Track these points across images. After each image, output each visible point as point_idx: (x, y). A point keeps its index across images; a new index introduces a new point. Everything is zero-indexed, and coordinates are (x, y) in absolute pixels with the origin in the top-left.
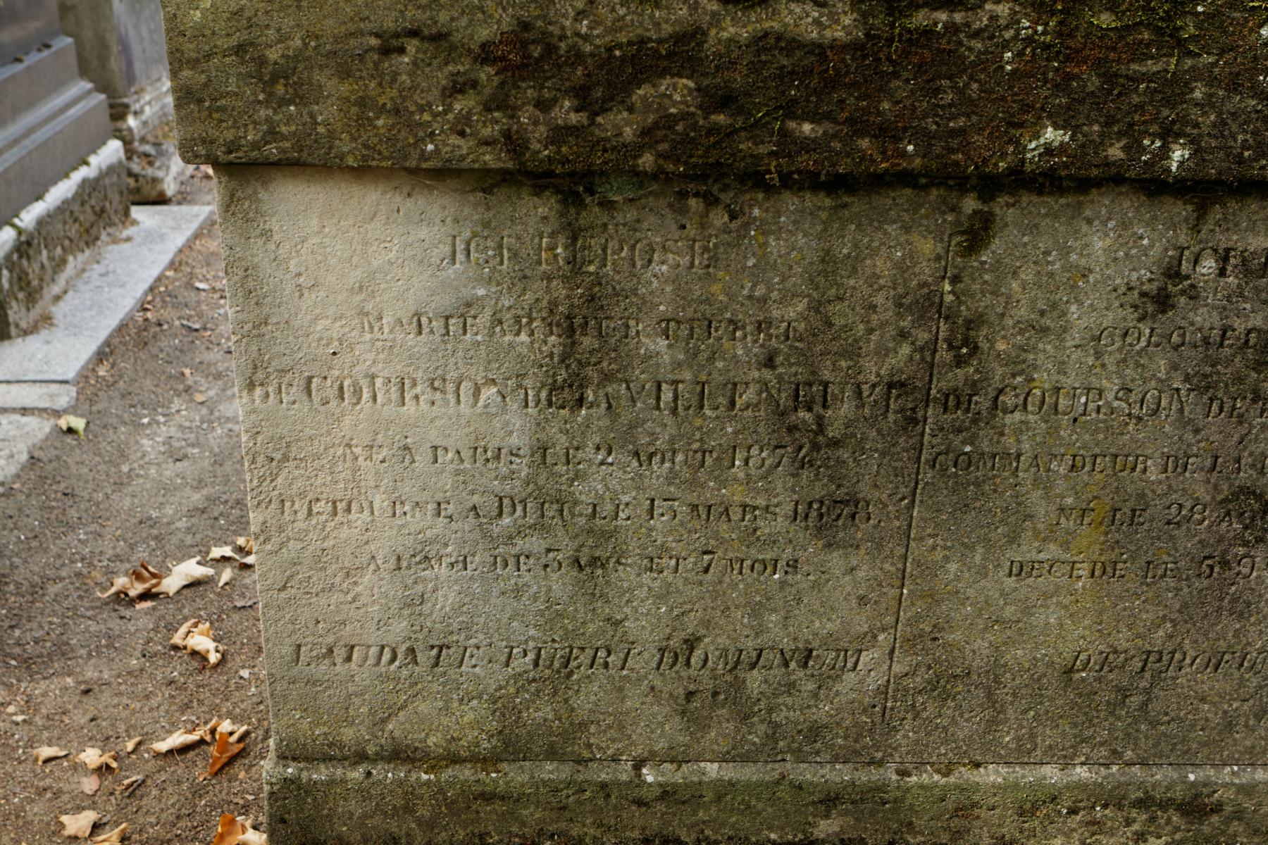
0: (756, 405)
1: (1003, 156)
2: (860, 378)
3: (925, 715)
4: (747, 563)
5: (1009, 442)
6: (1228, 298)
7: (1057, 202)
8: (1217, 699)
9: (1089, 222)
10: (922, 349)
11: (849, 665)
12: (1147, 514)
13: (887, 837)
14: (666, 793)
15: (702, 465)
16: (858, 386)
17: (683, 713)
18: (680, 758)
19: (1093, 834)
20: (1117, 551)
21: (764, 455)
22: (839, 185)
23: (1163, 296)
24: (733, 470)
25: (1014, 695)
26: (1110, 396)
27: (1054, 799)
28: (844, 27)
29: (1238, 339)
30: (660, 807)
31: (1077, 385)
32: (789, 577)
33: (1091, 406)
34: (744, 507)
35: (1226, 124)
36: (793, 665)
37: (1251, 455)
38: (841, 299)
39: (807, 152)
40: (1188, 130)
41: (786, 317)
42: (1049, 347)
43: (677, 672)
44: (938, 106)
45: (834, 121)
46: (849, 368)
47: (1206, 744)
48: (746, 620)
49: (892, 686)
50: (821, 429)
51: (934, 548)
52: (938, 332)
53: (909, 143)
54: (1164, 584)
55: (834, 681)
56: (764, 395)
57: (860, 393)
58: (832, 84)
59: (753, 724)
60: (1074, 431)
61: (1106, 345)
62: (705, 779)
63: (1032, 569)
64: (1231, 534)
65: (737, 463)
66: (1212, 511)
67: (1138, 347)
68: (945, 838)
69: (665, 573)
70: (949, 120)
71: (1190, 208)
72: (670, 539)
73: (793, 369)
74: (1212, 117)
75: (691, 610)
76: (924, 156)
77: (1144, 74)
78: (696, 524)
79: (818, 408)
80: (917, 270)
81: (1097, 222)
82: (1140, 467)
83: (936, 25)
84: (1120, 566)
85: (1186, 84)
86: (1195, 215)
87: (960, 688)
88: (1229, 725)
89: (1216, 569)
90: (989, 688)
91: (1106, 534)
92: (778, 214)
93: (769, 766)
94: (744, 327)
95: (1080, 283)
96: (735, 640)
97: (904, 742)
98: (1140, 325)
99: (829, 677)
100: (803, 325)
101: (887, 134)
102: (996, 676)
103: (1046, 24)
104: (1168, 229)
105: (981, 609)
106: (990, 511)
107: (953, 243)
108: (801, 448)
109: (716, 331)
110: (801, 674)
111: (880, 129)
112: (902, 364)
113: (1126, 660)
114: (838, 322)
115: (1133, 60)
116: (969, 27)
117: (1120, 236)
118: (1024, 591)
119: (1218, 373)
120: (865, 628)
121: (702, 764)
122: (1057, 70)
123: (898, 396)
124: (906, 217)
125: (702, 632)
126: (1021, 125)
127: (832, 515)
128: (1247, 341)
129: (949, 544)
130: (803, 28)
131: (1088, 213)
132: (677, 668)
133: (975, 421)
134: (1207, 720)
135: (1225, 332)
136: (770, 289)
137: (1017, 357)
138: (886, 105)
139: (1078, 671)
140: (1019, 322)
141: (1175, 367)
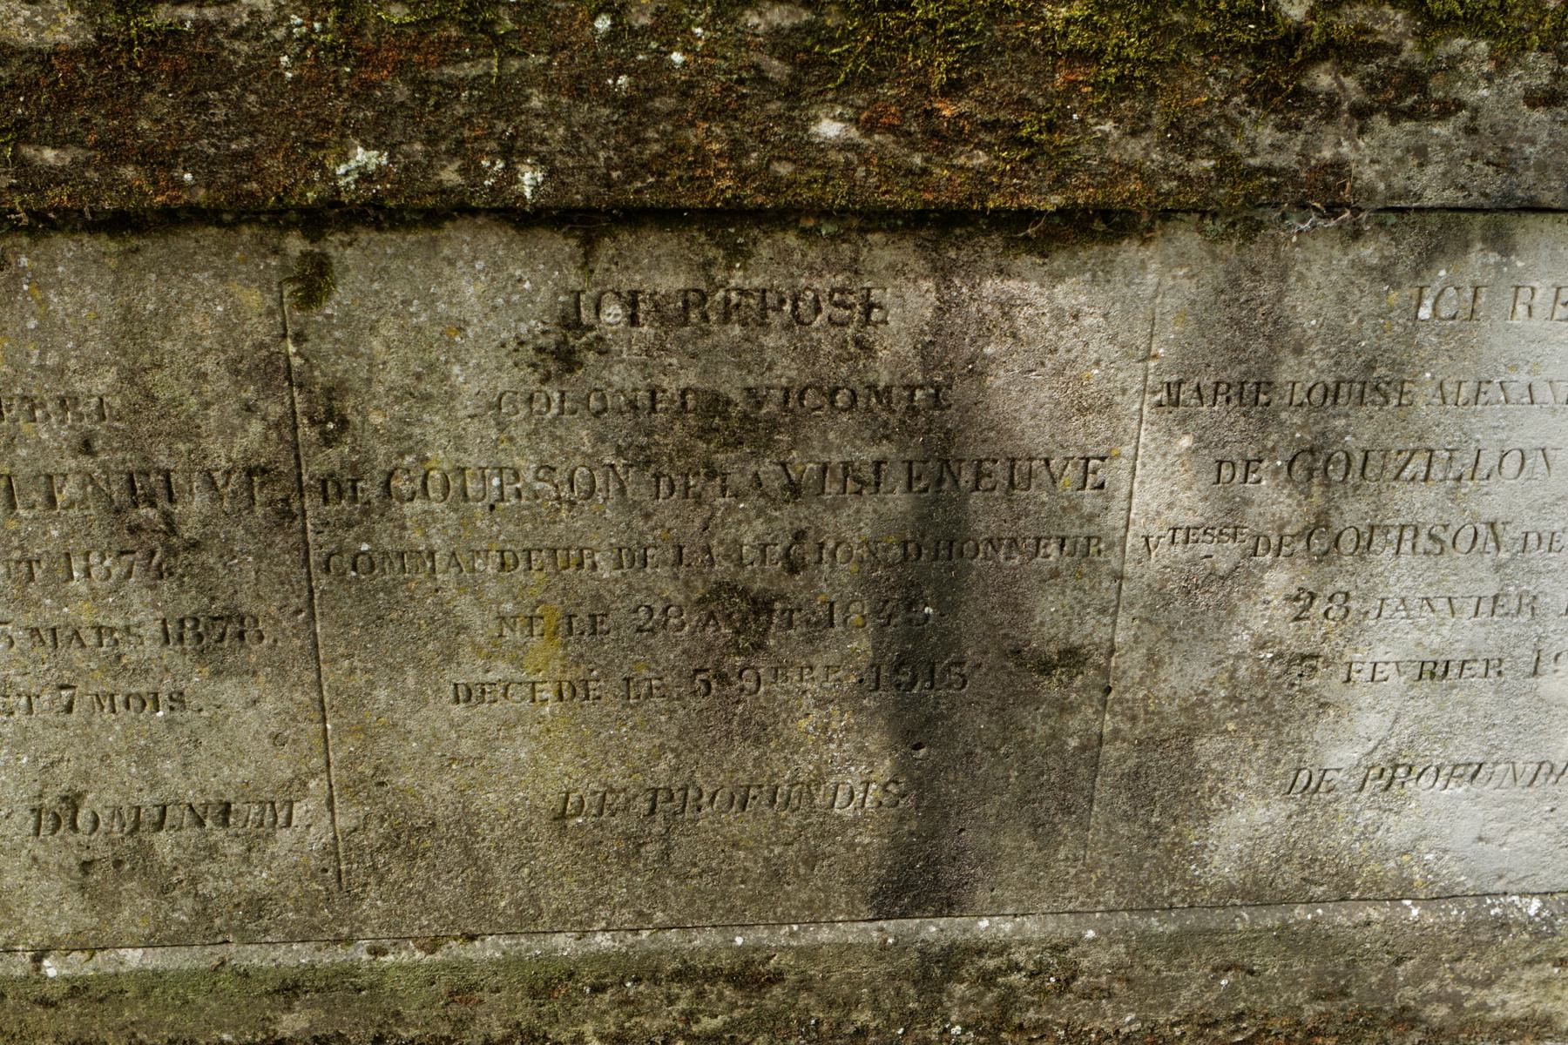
0: (82, 502)
1: (309, 183)
2: (208, 463)
3: (391, 878)
4: (119, 699)
5: (415, 536)
6: (647, 352)
7: (404, 239)
8: (752, 843)
9: (451, 263)
10: (277, 426)
11: (281, 820)
12: (610, 621)
13: (372, 1031)
14: (77, 989)
15: (32, 578)
16: (209, 473)
17: (82, 888)
18: (91, 944)
19: (630, 1016)
20: (583, 667)
21: (107, 563)
22: (120, 224)
23: (564, 351)
24: (73, 583)
25: (498, 848)
26: (528, 476)
27: (571, 975)
28: (67, 29)
29: (672, 401)
30: (72, 1007)
31: (483, 464)
32: (177, 714)
33: (508, 489)
34: (99, 629)
35: (579, 139)
36: (208, 823)
37: (721, 542)
38: (160, 367)
39: (58, 184)
40: (535, 146)
41: (94, 391)
42: (437, 419)
43: (61, 838)
44: (211, 123)
45: (82, 145)
46: (190, 452)
47: (752, 900)
48: (133, 770)
49: (341, 844)
50: (171, 528)
51: (352, 671)
52: (293, 403)
53: (185, 169)
54: (651, 706)
55: (266, 840)
56: (89, 489)
57: (214, 483)
58: (67, 99)
59: (175, 900)
60: (493, 522)
61: (508, 414)
62: (123, 969)
63: (483, 691)
64: (721, 642)
65: (75, 574)
66: (690, 613)
67: (549, 416)
68: (445, 1030)
69: (17, 715)
70: (230, 140)
71: (573, 242)
72: (12, 672)
73: (119, 455)
74: (561, 131)
75: (61, 760)
76: (208, 187)
77: (462, 80)
78: (41, 652)
79: (163, 503)
80: (247, 328)
81: (460, 263)
82: (587, 562)
83: (182, 23)
84: (592, 685)
85: (518, 91)
86: (582, 251)
87: (428, 843)
88: (776, 876)
89: (714, 685)
90: (464, 841)
91: (565, 646)
92: (53, 263)
93: (208, 950)
94: (43, 405)
95: (458, 339)
96: (127, 795)
97: (373, 913)
98: (545, 388)
99: (258, 836)
100: (118, 400)
101: (155, 159)
102: (470, 828)
103: (324, 21)
104: (552, 269)
105: (430, 746)
106: (411, 622)
107: (286, 293)
108: (153, 553)
109: (9, 411)
110: (222, 834)
111: (143, 155)
112: (256, 445)
113: (628, 800)
114: (163, 395)
115: (443, 63)
116: (226, 25)
117: (493, 279)
118: (479, 720)
119: (657, 444)
120: (289, 774)
121: (122, 952)
122: (351, 76)
123: (262, 485)
124: (218, 263)
125: (81, 787)
126: (321, 145)
127: (215, 633)
128: (684, 404)
129: (370, 665)
130: (14, 30)
131: (447, 252)
132: (60, 833)
133: (366, 513)
134: (746, 870)
135: (653, 394)
136: (65, 357)
137: (400, 431)
138: (144, 124)
139: (572, 816)
140: (391, 389)
141: (601, 439)
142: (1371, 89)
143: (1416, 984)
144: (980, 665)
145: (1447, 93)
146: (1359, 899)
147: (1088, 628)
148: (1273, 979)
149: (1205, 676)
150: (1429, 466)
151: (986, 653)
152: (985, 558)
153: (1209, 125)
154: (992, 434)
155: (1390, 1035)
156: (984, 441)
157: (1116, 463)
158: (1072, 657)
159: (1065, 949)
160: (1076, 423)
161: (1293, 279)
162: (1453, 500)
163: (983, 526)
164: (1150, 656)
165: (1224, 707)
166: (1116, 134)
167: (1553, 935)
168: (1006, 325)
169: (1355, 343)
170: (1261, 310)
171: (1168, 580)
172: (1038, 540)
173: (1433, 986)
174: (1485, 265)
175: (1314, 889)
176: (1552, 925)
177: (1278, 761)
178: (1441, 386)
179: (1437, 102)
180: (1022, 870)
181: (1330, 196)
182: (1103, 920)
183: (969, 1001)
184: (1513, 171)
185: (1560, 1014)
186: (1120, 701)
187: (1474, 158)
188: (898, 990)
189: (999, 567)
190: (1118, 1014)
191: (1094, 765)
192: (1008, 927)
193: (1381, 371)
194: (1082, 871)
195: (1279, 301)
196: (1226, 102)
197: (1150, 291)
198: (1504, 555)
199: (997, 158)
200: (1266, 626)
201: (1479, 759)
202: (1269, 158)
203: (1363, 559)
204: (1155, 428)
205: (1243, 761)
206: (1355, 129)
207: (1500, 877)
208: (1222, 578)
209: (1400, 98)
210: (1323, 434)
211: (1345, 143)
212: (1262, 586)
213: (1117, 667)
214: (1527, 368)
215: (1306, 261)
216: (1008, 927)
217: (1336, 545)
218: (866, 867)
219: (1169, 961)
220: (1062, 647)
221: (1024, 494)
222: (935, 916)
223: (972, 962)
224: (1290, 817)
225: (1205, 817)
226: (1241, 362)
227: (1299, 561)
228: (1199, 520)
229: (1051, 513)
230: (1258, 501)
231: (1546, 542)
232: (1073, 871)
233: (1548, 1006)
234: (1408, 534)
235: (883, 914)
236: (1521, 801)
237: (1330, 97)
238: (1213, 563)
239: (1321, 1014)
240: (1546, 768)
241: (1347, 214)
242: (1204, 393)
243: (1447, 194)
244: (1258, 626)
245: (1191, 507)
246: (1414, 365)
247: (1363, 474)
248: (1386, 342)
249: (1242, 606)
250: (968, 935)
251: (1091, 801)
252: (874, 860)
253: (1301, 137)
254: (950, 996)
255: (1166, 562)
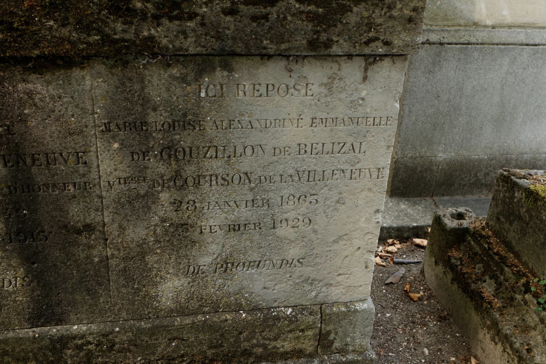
142: (158, 8)
143: (248, 341)
144: (51, 232)
145: (190, 10)
146: (222, 312)
147: (92, 217)
148: (192, 342)
149: (144, 233)
150: (217, 152)
151: (52, 227)
152: (44, 191)
153: (94, 22)
154: (35, 144)
155: (242, 359)
156: (33, 147)
157: (89, 154)
158: (89, 228)
159: (107, 335)
160: (69, 139)
161: (147, 82)
162: (228, 165)
163: (40, 179)
164: (120, 226)
165: (154, 244)
166: (56, 26)
167: (297, 321)
168: (31, 102)
169: (177, 106)
170: (136, 94)
171: (121, 198)
172: (64, 184)
173: (255, 341)
174: (223, 76)
175: (204, 308)
176: (296, 318)
177: (180, 263)
178: (215, 122)
179: (186, 13)
180: (87, 307)
181: (149, 48)
182: (123, 324)
183: (74, 356)
184: (223, 40)
185: (305, 349)
186: (112, 243)
187: (206, 35)
188: (44, 354)
189: (50, 195)
190: (135, 358)
191: (107, 267)
192: (84, 328)
193: (190, 117)
194: (111, 307)
195: (143, 91)
196: (99, 13)
197: (88, 88)
198: (253, 185)
199: (7, 36)
200: (164, 214)
201: (258, 259)
202: (122, 35)
203: (197, 188)
204: (103, 140)
205: (166, 264)
206: (155, 24)
207: (276, 301)
208: (143, 196)
209: (172, 12)
210: (172, 141)
211: (152, 30)
212: (159, 199)
213: (107, 231)
214: (247, 115)
215: (150, 75)
216: (84, 328)
217: (186, 183)
218: (23, 309)
219: (150, 338)
220: (83, 224)
221: (54, 167)
222: (56, 325)
223: (72, 342)
224: (189, 283)
225: (156, 284)
226: (132, 115)
227: (172, 189)
228: (130, 175)
229: (67, 174)
230: (150, 167)
231: (268, 179)
232: (107, 307)
233: (300, 346)
234: (214, 178)
235: (34, 325)
236: (278, 274)
237: (142, 10)
238: (138, 191)
239: (214, 353)
240: (285, 262)
241: (160, 57)
242: (120, 126)
243: (198, 49)
244: (161, 213)
245: (124, 170)
246: (202, 114)
247: (191, 156)
248: (189, 106)
249: (153, 207)
250: (68, 332)
251: (109, 281)
252: (26, 306)
253: (134, 27)
254: (66, 355)
255: (118, 191)
